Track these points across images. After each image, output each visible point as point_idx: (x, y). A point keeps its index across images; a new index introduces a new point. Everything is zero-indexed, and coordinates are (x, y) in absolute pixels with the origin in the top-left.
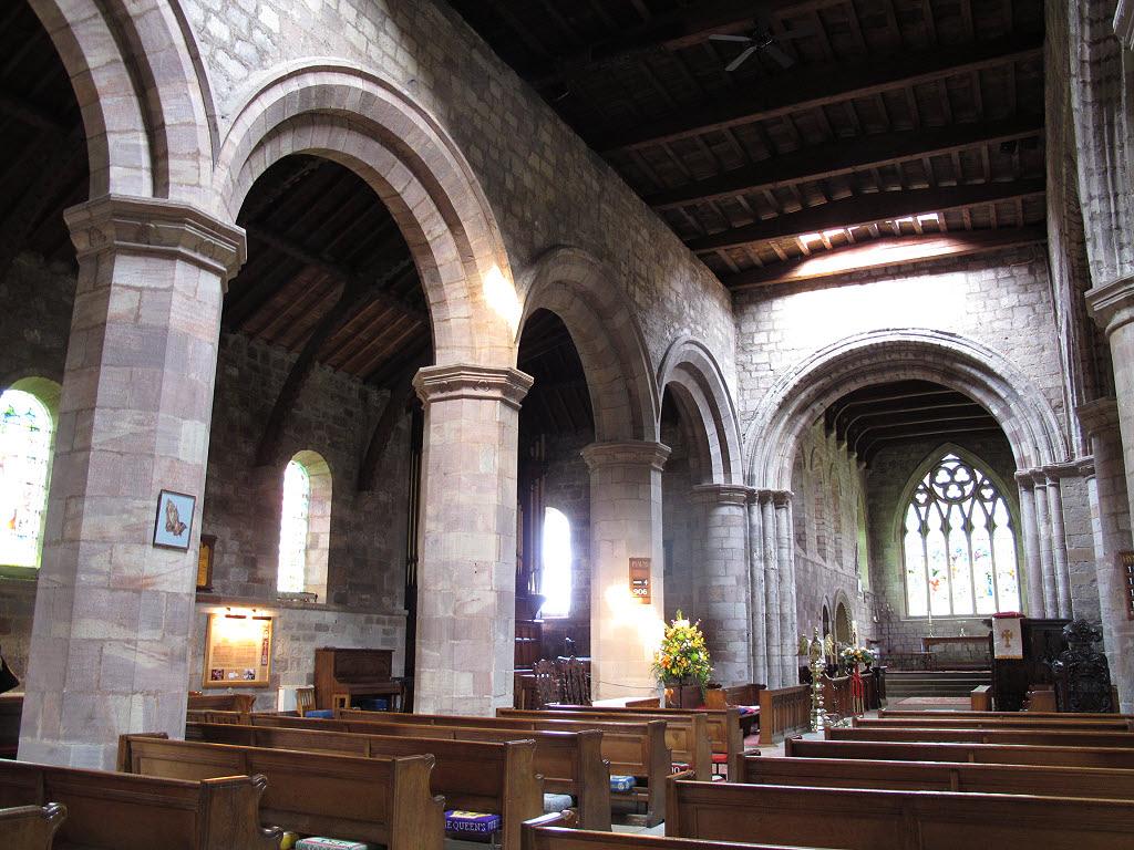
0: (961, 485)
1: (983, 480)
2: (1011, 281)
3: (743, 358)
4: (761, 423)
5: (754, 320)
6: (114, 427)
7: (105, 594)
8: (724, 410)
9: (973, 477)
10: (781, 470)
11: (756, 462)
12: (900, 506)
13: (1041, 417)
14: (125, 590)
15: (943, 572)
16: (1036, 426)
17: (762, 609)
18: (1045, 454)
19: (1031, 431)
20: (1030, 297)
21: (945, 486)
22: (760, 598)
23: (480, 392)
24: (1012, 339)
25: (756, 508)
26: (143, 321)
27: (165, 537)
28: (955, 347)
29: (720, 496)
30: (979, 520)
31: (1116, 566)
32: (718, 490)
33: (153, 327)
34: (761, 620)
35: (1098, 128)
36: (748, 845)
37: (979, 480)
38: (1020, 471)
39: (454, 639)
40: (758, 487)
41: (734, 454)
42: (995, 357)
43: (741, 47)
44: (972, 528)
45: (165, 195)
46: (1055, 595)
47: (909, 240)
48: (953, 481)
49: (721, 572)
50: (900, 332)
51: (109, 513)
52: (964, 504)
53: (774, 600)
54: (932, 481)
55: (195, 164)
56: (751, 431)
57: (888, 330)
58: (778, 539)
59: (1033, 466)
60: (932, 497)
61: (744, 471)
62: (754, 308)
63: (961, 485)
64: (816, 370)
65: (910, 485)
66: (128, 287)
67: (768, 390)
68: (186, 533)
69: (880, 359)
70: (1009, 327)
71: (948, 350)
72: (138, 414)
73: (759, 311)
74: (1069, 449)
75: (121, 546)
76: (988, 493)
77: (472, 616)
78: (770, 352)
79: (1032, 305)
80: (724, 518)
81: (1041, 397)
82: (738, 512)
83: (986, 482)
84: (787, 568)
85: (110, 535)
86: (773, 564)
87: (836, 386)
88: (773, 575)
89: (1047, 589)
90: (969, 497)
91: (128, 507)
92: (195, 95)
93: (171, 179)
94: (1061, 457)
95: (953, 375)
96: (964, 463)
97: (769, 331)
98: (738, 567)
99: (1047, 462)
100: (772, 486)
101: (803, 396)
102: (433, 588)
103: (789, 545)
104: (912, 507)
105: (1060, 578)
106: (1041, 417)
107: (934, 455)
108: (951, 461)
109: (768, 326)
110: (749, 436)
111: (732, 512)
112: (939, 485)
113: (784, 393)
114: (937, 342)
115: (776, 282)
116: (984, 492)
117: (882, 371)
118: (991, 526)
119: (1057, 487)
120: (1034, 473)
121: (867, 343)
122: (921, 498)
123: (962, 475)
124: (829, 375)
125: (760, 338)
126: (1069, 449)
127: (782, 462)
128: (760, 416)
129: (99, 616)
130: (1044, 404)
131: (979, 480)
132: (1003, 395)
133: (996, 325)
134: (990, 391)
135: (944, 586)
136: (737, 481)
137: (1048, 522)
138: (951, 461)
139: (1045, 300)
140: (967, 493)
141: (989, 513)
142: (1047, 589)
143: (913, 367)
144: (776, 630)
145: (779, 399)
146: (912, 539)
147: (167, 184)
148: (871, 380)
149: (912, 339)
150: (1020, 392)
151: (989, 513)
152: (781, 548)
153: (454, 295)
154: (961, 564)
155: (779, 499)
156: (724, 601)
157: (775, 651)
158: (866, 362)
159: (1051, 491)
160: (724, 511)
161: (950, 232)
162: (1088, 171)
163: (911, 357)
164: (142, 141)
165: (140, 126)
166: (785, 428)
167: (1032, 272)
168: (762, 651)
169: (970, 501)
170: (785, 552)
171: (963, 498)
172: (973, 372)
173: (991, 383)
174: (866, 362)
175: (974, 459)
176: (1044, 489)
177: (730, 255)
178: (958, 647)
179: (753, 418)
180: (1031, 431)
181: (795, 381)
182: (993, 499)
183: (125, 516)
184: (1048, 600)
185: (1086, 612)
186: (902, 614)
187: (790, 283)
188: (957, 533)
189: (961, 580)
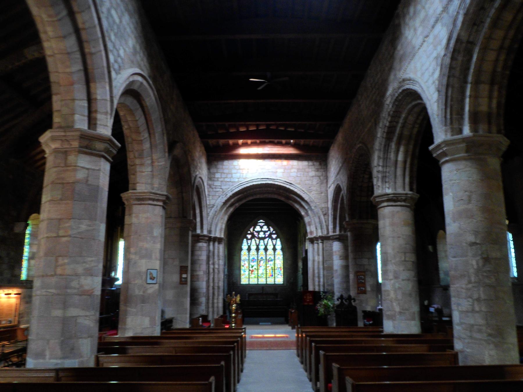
0: (265, 232)
2: (313, 167)
3: (210, 182)
4: (216, 210)
6: (79, 227)
7: (77, 298)
8: (204, 204)
11: (213, 225)
13: (319, 218)
14: (85, 295)
15: (255, 267)
16: (317, 220)
18: (319, 231)
19: (315, 222)
20: (319, 173)
21: (258, 232)
23: (155, 203)
24: (312, 188)
25: (211, 243)
26: (89, 182)
27: (150, 281)
28: (291, 188)
29: (198, 238)
30: (270, 247)
32: (198, 236)
34: (211, 288)
35: (385, 146)
39: (143, 304)
40: (213, 235)
41: (205, 222)
42: (305, 194)
45: (95, 129)
46: (319, 282)
48: (262, 231)
49: (198, 269)
52: (265, 240)
53: (216, 280)
55: (105, 117)
56: (212, 213)
58: (218, 256)
59: (314, 235)
60: (253, 236)
62: (216, 163)
64: (239, 191)
67: (219, 196)
74: (328, 229)
75: (83, 277)
76: (274, 236)
78: (222, 181)
79: (319, 176)
80: (200, 247)
81: (320, 210)
82: (205, 245)
83: (274, 232)
85: (79, 272)
86: (216, 266)
87: (245, 197)
88: (216, 271)
89: (316, 279)
92: (108, 88)
93: (98, 122)
94: (325, 233)
95: (289, 198)
98: (204, 267)
99: (320, 234)
100: (218, 235)
101: (233, 200)
102: (133, 282)
104: (245, 240)
105: (321, 275)
106: (319, 218)
108: (261, 223)
109: (221, 171)
110: (211, 214)
111: (203, 245)
113: (225, 199)
115: (226, 154)
118: (274, 249)
119: (323, 243)
120: (315, 237)
121: (259, 183)
122: (249, 236)
123: (265, 228)
125: (218, 175)
126: (328, 229)
127: (222, 226)
128: (215, 207)
130: (320, 213)
132: (306, 207)
133: (307, 182)
134: (302, 206)
136: (205, 233)
137: (318, 255)
138: (261, 223)
140: (267, 236)
142: (316, 279)
144: (216, 293)
146: (244, 253)
147: (95, 124)
149: (276, 183)
150: (313, 208)
152: (219, 260)
155: (220, 240)
157: (215, 301)
159: (321, 245)
160: (200, 244)
161: (294, 146)
162: (379, 157)
165: (86, 98)
166: (224, 212)
167: (320, 164)
168: (211, 301)
169: (268, 238)
173: (303, 203)
174: (258, 190)
176: (318, 243)
177: (212, 142)
179: (213, 207)
180: (315, 222)
182: (276, 239)
183: (84, 264)
184: (317, 283)
185: (330, 288)
187: (231, 155)
188: (262, 252)
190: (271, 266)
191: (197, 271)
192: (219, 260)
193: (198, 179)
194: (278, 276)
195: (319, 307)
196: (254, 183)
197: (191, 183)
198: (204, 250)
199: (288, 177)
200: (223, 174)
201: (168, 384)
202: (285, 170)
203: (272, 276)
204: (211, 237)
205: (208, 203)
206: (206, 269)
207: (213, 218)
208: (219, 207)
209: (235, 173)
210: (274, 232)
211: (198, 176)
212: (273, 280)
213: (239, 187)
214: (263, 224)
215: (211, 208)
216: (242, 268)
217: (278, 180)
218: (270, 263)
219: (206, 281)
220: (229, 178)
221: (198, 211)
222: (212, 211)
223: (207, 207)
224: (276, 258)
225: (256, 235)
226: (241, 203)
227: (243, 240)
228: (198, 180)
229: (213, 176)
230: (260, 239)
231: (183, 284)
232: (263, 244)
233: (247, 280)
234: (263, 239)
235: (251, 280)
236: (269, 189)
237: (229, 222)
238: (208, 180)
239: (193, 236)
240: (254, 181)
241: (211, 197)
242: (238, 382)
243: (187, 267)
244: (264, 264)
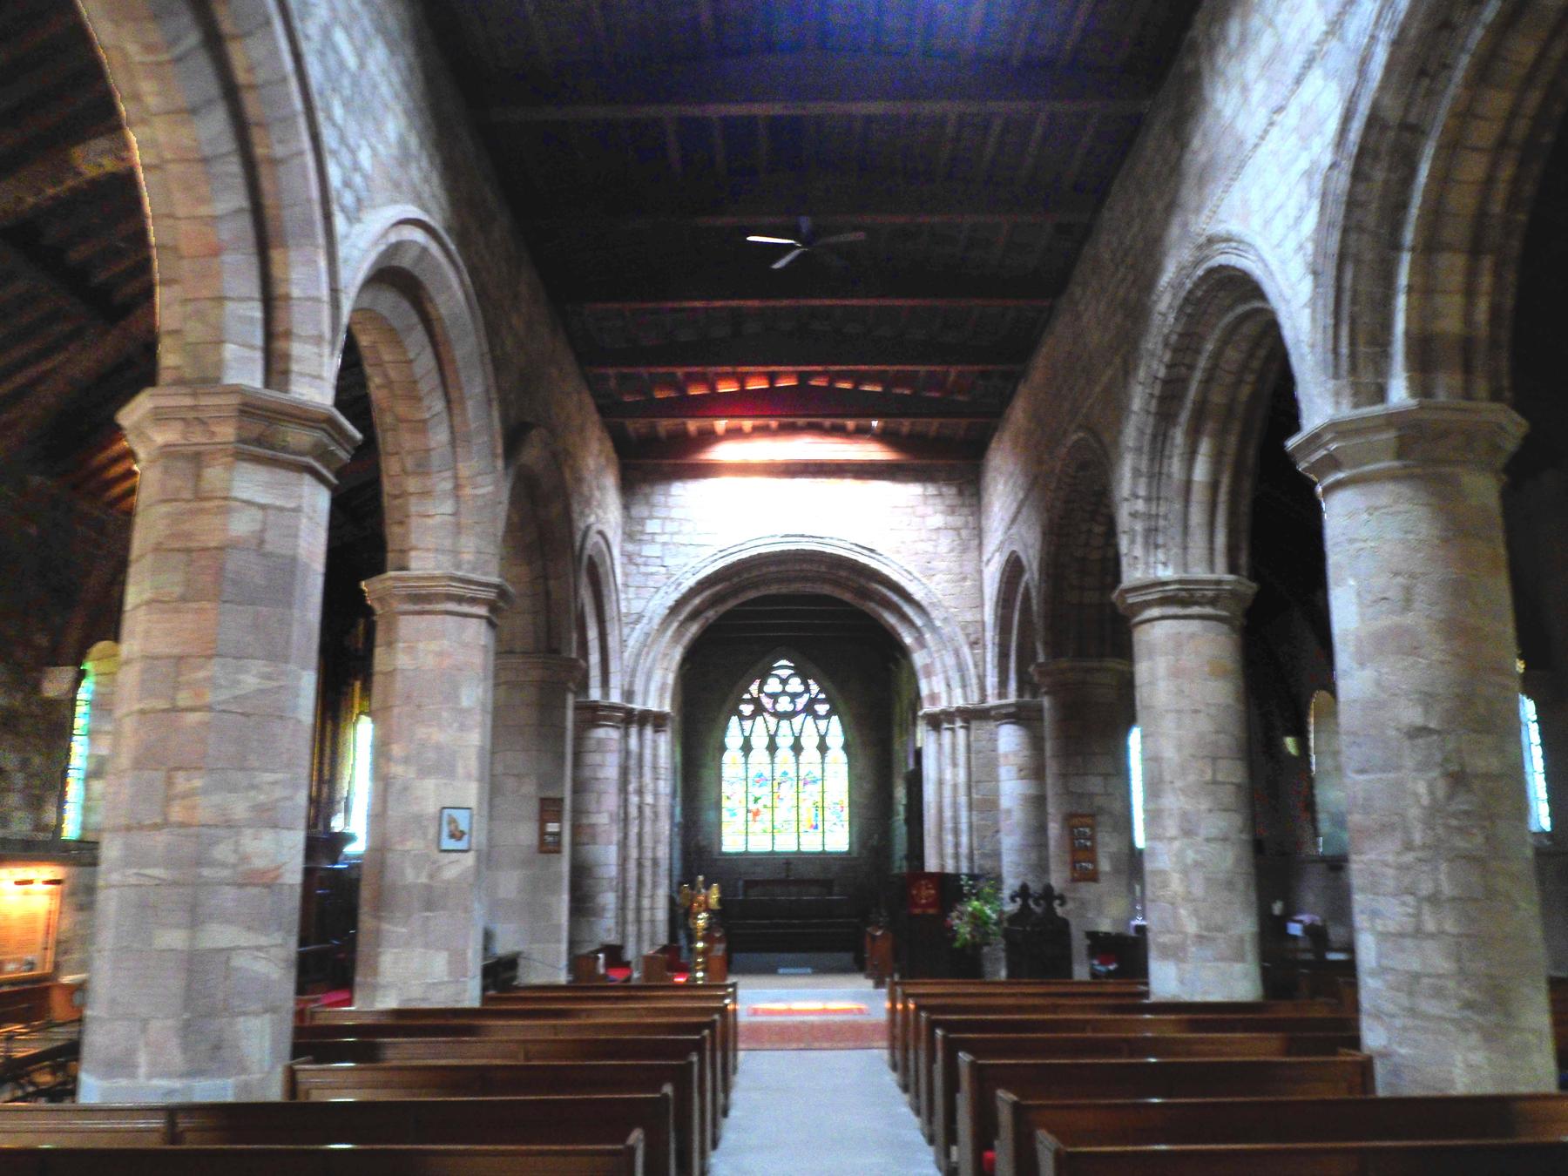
2: (938, 501)
3: (630, 547)
6: (238, 682)
7: (230, 893)
8: (610, 611)
13: (957, 653)
14: (255, 885)
16: (950, 661)
17: (634, 853)
18: (958, 692)
19: (944, 665)
20: (957, 521)
21: (774, 697)
23: (465, 608)
24: (935, 564)
25: (634, 731)
26: (268, 547)
28: (874, 564)
29: (593, 715)
30: (810, 742)
31: (1063, 828)
32: (594, 707)
33: (283, 556)
34: (632, 865)
35: (1154, 437)
36: (255, 1146)
38: (927, 708)
39: (428, 910)
40: (637, 706)
41: (614, 666)
42: (916, 582)
43: (790, 247)
45: (284, 386)
46: (957, 845)
47: (837, 437)
48: (784, 693)
49: (593, 807)
51: (233, 789)
53: (648, 842)
55: (315, 350)
56: (634, 638)
57: (803, 536)
58: (655, 768)
59: (943, 705)
60: (759, 709)
62: (647, 490)
64: (716, 573)
66: (249, 503)
67: (658, 589)
68: (466, 838)
70: (931, 549)
72: (265, 666)
73: (652, 493)
74: (983, 689)
75: (249, 832)
76: (822, 709)
77: (449, 882)
78: (664, 544)
79: (957, 529)
80: (600, 741)
81: (958, 630)
82: (614, 734)
83: (822, 696)
86: (649, 799)
88: (648, 812)
89: (949, 838)
90: (800, 712)
91: (256, 781)
92: (323, 263)
94: (974, 698)
95: (867, 595)
98: (611, 801)
99: (959, 702)
100: (653, 706)
101: (697, 601)
102: (399, 847)
104: (734, 720)
105: (964, 826)
106: (957, 653)
108: (783, 667)
110: (631, 642)
111: (608, 734)
113: (676, 596)
115: (678, 462)
117: (789, 580)
118: (823, 748)
119: (967, 728)
120: (944, 712)
122: (747, 709)
123: (795, 685)
124: (729, 580)
125: (652, 526)
126: (983, 689)
127: (665, 677)
128: (645, 620)
129: (227, 920)
130: (961, 639)
132: (919, 622)
134: (904, 618)
135: (766, 815)
136: (615, 698)
137: (955, 765)
138: (783, 667)
139: (971, 525)
142: (949, 838)
143: (825, 581)
144: (648, 879)
145: (670, 602)
146: (731, 760)
147: (286, 373)
148: (774, 589)
149: (828, 550)
150: (938, 623)
152: (657, 779)
154: (787, 791)
155: (657, 721)
157: (646, 903)
159: (961, 734)
160: (601, 733)
161: (883, 437)
164: (258, 314)
165: (256, 294)
166: (672, 637)
167: (960, 493)
168: (631, 904)
170: (662, 784)
171: (794, 714)
172: (890, 594)
173: (909, 610)
174: (773, 569)
176: (952, 730)
177: (635, 426)
179: (637, 621)
181: (690, 582)
182: (828, 716)
183: (252, 793)
184: (949, 850)
185: (988, 864)
187: (692, 464)
188: (785, 753)
189: (785, 812)
192: (656, 779)
193: (594, 538)
195: (957, 921)
204: (633, 709)
206: (619, 807)
207: (638, 655)
208: (657, 621)
211: (595, 528)
221: (592, 634)
222: (636, 634)
226: (722, 609)
228: (595, 540)
229: (639, 528)
230: (780, 716)
231: (550, 852)
234: (788, 716)
237: (688, 666)
238: (624, 541)
243: (561, 800)
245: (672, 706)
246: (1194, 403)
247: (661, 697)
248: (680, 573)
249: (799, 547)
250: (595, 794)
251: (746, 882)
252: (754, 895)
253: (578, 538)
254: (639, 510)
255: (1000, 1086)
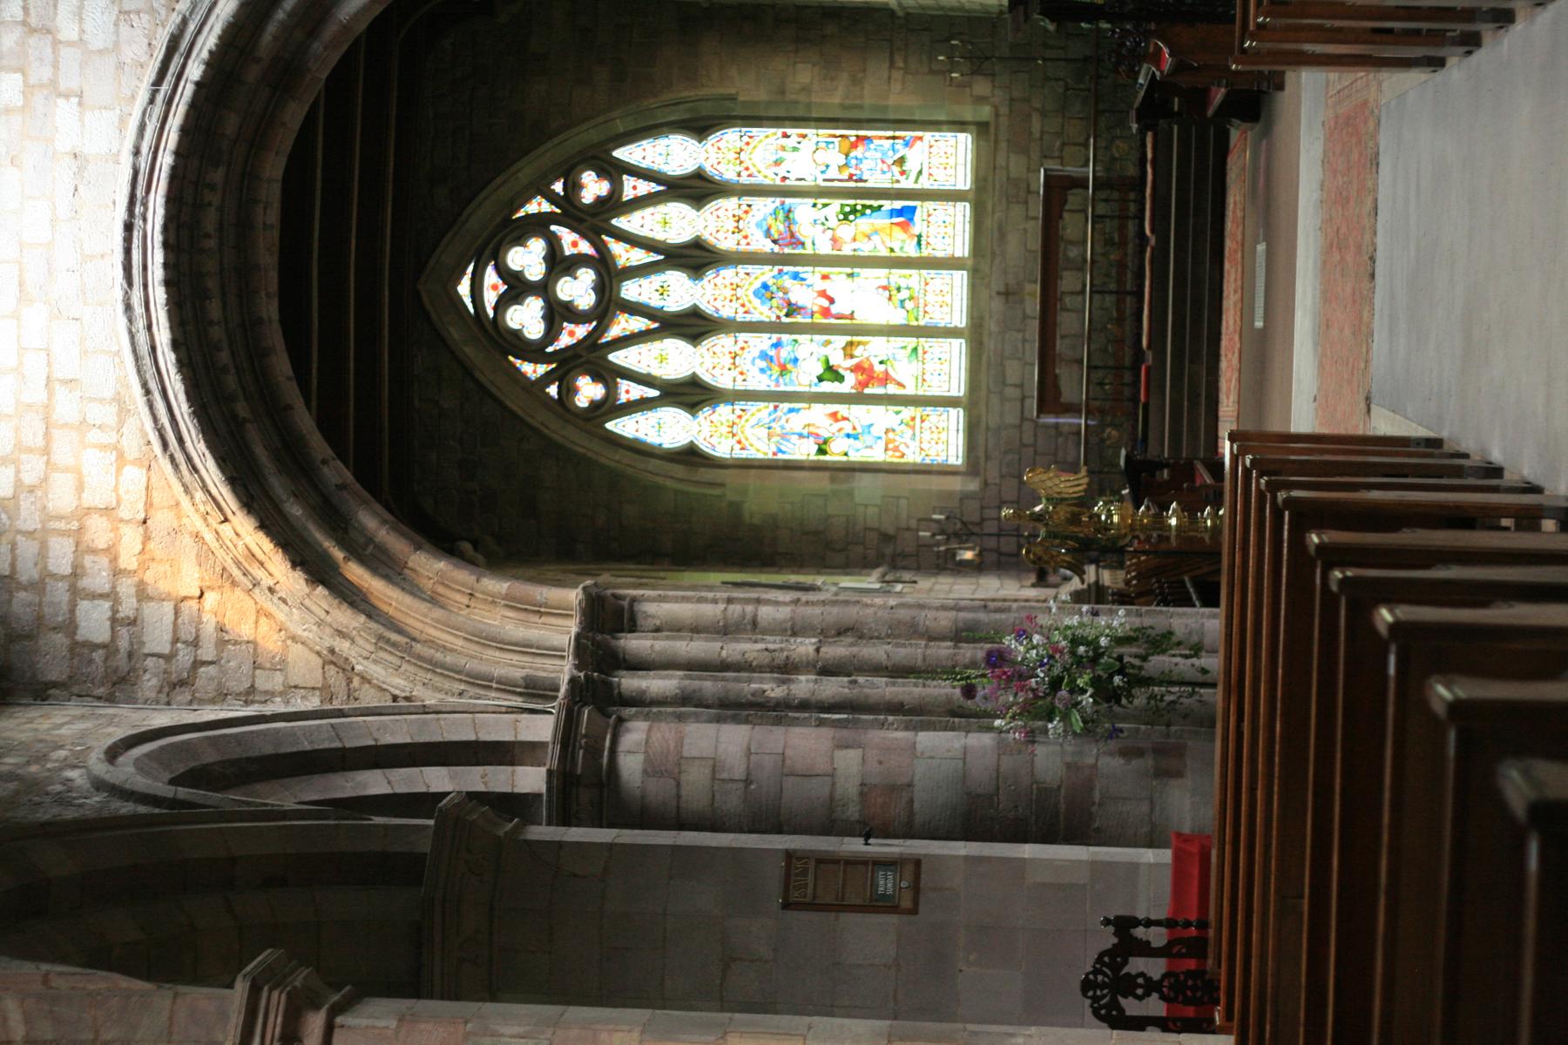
0: (559, 264)
1: (552, 198)
3: (149, 683)
5: (29, 637)
8: (319, 736)
9: (539, 225)
10: (515, 604)
11: (483, 668)
12: (609, 458)
21: (558, 313)
22: (908, 690)
25: (630, 683)
28: (209, 41)
32: (564, 782)
37: (546, 207)
40: (563, 671)
41: (458, 730)
44: (698, 245)
48: (544, 289)
49: (818, 789)
50: (140, 193)
53: (905, 653)
54: (534, 351)
58: (725, 630)
61: (511, 710)
63: (559, 264)
64: (222, 461)
65: (540, 419)
69: (210, 265)
71: (216, 62)
76: (593, 187)
80: (652, 769)
84: (817, 610)
86: (804, 647)
88: (837, 651)
90: (601, 248)
96: (491, 250)
97: (76, 593)
100: (564, 632)
101: (295, 510)
103: (747, 601)
104: (622, 427)
107: (455, 333)
110: (399, 683)
112: (552, 332)
114: (187, 91)
116: (588, 196)
121: (159, 295)
122: (588, 391)
123: (528, 258)
128: (343, 646)
131: (546, 207)
135: (874, 350)
136: (541, 728)
140: (585, 247)
141: (654, 187)
149: (166, 160)
151: (654, 187)
152: (754, 623)
153: (179, 698)
156: (910, 785)
158: (214, 309)
160: (631, 765)
163: (217, 176)
166: (386, 577)
174: (214, 309)
175: (479, 216)
178: (1067, 322)
179: (346, 668)
182: (614, 171)
186: (956, 484)
190: (833, 222)
191: (832, 797)
192: (754, 627)
193: (126, 771)
194: (912, 165)
195: (51, 609)
196: (163, 336)
197: (148, 820)
198: (680, 742)
199: (121, 65)
200: (84, 583)
201: (1393, 872)
202: (62, 86)
203: (907, 213)
204: (573, 681)
205: (313, 703)
206: (821, 723)
207: (434, 666)
208: (345, 617)
209: (80, 488)
210: (558, 187)
211: (100, 768)
212: (941, 210)
213: (189, 459)
214: (491, 276)
215: (349, 681)
216: (838, 452)
217: (145, 149)
218: (804, 230)
219: (917, 728)
220: (118, 539)
221: (376, 783)
222: (377, 672)
223: (340, 713)
224: (768, 177)
225: (581, 331)
226: (318, 446)
227: (617, 441)
228: (131, 769)
229: (98, 656)
230: (608, 303)
231: (916, 888)
232: (656, 280)
233: (935, 415)
234: (609, 276)
235: (936, 389)
236: (210, 222)
237: (466, 546)
238: (131, 700)
239: (565, 818)
240: (142, 338)
241: (263, 682)
242: (1536, 489)
243: (789, 855)
244: (812, 274)
245: (574, 586)
246: (211, 52)
247: (540, 610)
248: (220, 553)
249: (158, 238)
250: (789, 783)
251: (1043, 408)
252: (1074, 385)
253: (127, 808)
254: (52, 662)
255: (1082, 21)
